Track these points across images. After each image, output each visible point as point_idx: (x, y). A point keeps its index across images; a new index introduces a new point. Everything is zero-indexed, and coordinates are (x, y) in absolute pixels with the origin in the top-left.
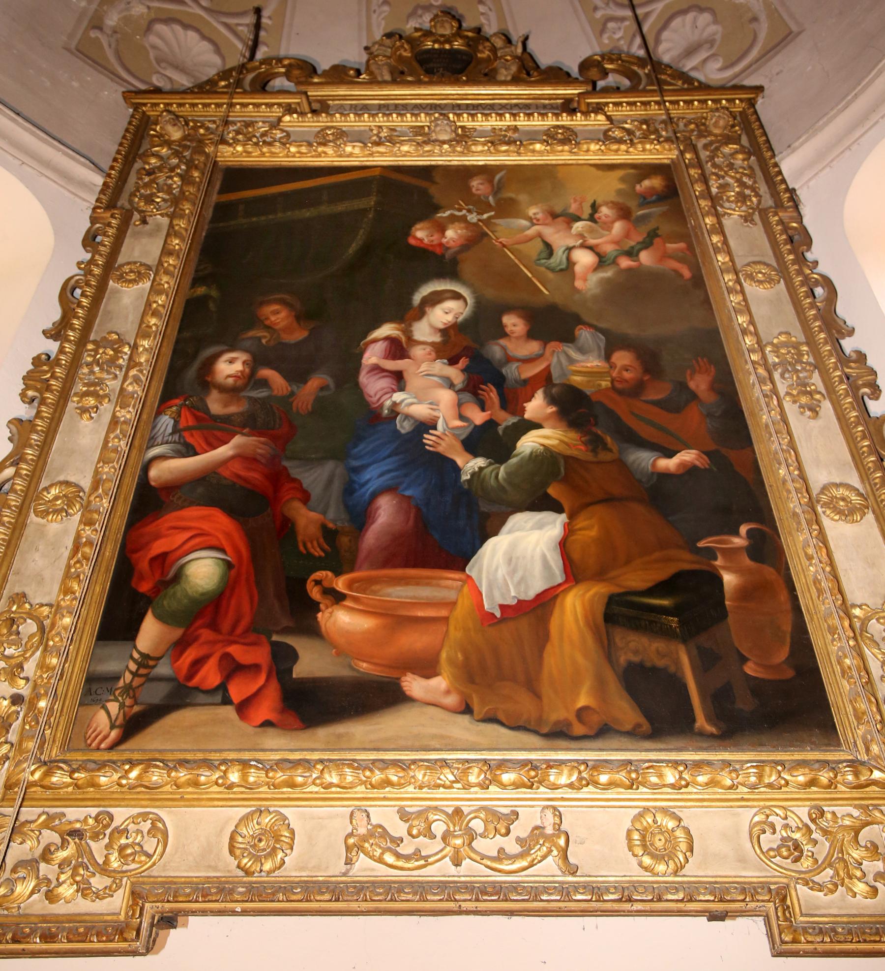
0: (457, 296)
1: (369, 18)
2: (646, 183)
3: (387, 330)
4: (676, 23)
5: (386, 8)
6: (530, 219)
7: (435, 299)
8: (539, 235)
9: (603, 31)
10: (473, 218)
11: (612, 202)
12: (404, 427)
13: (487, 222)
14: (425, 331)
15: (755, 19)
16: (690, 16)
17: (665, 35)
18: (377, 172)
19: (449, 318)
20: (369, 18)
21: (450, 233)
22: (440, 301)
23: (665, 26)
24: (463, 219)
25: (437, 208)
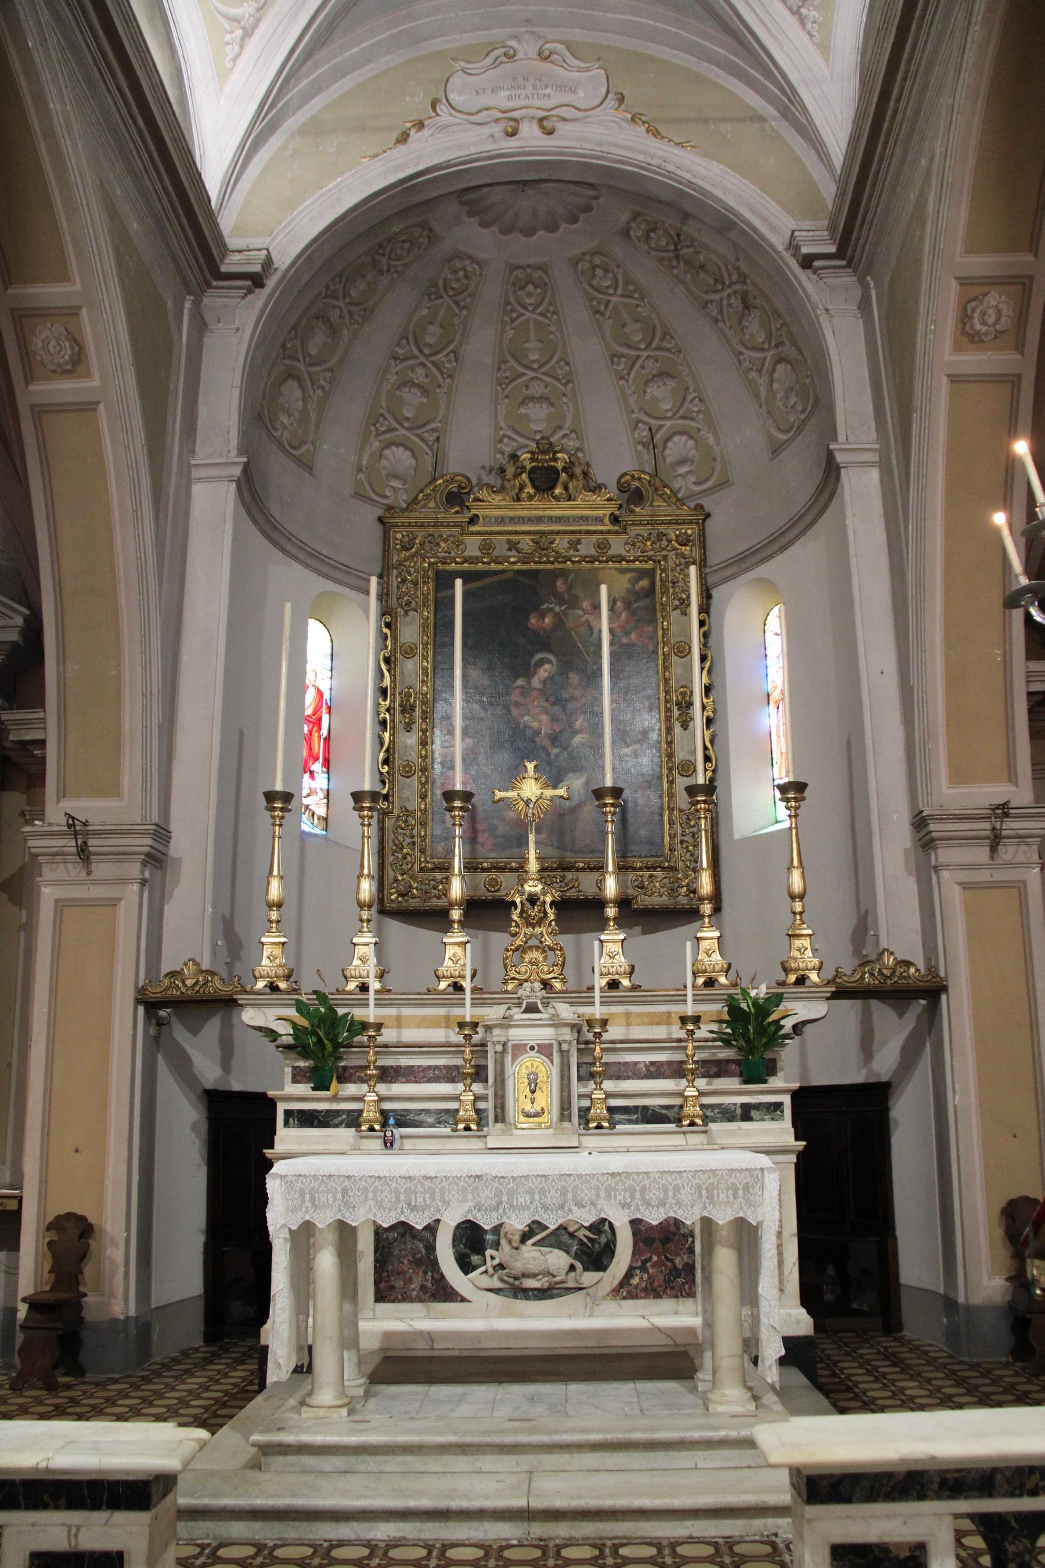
0: (550, 662)
1: (496, 408)
2: (641, 583)
3: (520, 682)
4: (676, 438)
5: (506, 400)
6: (583, 610)
7: (542, 662)
8: (587, 621)
9: (635, 428)
10: (557, 609)
11: (623, 598)
12: (528, 733)
13: (564, 612)
14: (536, 682)
15: (714, 459)
16: (684, 438)
17: (670, 444)
18: (511, 574)
19: (546, 674)
20: (496, 408)
21: (547, 620)
22: (543, 664)
23: (669, 439)
24: (552, 610)
25: (542, 603)
